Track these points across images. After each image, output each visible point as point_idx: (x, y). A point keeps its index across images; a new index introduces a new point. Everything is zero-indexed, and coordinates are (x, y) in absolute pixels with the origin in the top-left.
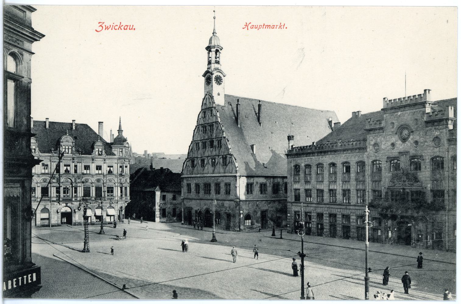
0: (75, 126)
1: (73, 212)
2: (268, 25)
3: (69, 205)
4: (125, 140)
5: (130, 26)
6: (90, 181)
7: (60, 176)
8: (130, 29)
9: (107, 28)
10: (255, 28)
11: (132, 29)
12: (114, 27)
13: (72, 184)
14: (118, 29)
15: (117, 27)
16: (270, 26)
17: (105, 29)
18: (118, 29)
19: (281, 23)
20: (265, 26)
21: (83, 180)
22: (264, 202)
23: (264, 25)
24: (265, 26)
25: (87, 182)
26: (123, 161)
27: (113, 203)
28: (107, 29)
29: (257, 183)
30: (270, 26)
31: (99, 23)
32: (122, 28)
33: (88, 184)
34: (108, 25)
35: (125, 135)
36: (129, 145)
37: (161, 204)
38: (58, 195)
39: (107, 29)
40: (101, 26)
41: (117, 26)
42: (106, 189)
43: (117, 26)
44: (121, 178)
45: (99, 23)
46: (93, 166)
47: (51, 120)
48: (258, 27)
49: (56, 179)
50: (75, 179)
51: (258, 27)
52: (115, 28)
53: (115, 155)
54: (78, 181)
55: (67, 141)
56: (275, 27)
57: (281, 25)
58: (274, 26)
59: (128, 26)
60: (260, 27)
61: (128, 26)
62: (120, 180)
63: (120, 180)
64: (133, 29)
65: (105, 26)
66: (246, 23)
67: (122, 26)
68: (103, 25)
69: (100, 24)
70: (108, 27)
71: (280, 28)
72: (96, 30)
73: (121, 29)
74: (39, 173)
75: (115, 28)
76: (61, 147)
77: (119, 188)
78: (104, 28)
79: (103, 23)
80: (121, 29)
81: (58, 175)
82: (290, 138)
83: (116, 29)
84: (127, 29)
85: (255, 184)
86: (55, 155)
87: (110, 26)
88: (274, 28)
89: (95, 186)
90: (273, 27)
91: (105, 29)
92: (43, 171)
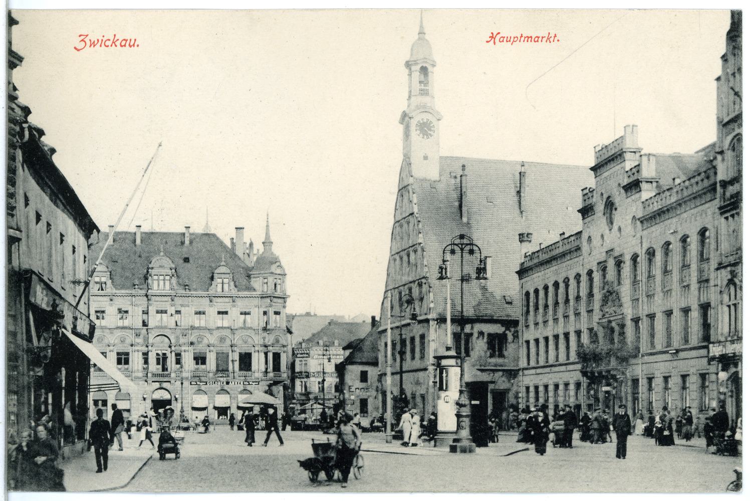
0: (188, 239)
1: (173, 399)
2: (528, 37)
3: (165, 385)
4: (275, 261)
5: (131, 40)
6: (205, 341)
7: (149, 331)
8: (130, 46)
9: (93, 44)
10: (507, 41)
11: (134, 45)
12: (103, 43)
13: (170, 347)
14: (111, 46)
15: (107, 43)
16: (531, 37)
17: (90, 46)
18: (111, 46)
19: (549, 33)
20: (523, 38)
21: (192, 338)
22: (501, 373)
23: (522, 36)
24: (523, 38)
25: (199, 342)
26: (269, 301)
27: (249, 384)
28: (93, 45)
29: (481, 333)
30: (531, 37)
31: (80, 36)
32: (118, 43)
33: (200, 348)
34: (94, 39)
35: (277, 250)
36: (284, 270)
37: (357, 390)
38: (145, 366)
39: (93, 45)
40: (83, 40)
41: (109, 40)
42: (237, 357)
43: (109, 40)
44: (265, 334)
45: (80, 36)
46: (212, 311)
47: (146, 228)
48: (512, 40)
49: (141, 336)
50: (177, 338)
51: (512, 40)
52: (106, 44)
53: (255, 290)
54: (182, 340)
55: (160, 266)
56: (540, 39)
57: (550, 36)
58: (539, 37)
59: (127, 40)
60: (516, 39)
61: (127, 40)
62: (264, 338)
63: (264, 338)
64: (136, 45)
65: (90, 40)
66: (492, 33)
67: (118, 40)
68: (87, 40)
69: (82, 37)
70: (94, 42)
71: (113, 44)
72: (75, 48)
73: (116, 46)
74: (113, 326)
75: (107, 44)
76: (150, 277)
77: (262, 356)
78: (88, 43)
79: (87, 36)
80: (116, 46)
81: (145, 330)
82: (523, 238)
83: (108, 46)
84: (125, 46)
85: (476, 335)
86: (140, 291)
87: (98, 40)
88: (538, 41)
89: (216, 350)
90: (537, 39)
91: (90, 46)
92: (120, 323)
